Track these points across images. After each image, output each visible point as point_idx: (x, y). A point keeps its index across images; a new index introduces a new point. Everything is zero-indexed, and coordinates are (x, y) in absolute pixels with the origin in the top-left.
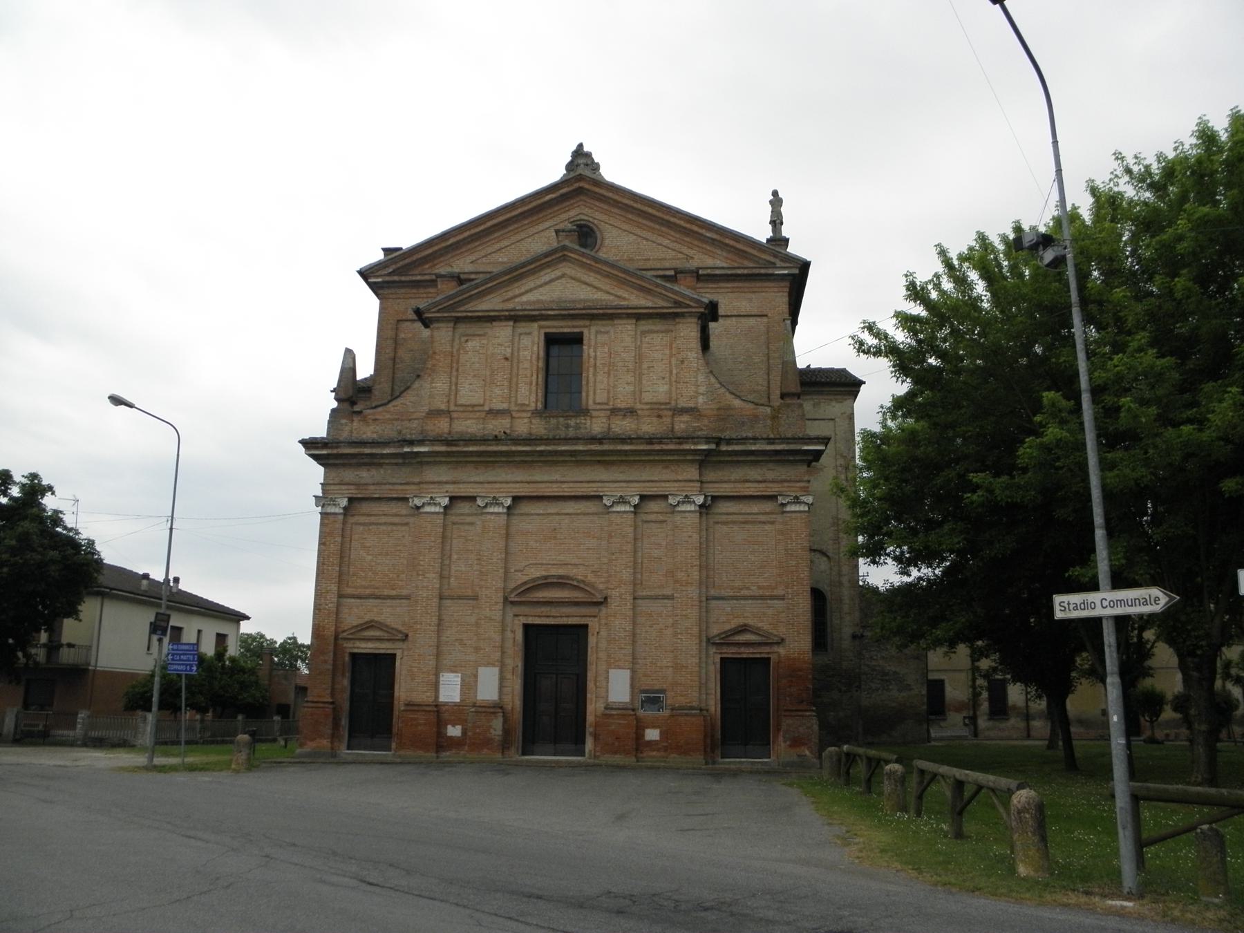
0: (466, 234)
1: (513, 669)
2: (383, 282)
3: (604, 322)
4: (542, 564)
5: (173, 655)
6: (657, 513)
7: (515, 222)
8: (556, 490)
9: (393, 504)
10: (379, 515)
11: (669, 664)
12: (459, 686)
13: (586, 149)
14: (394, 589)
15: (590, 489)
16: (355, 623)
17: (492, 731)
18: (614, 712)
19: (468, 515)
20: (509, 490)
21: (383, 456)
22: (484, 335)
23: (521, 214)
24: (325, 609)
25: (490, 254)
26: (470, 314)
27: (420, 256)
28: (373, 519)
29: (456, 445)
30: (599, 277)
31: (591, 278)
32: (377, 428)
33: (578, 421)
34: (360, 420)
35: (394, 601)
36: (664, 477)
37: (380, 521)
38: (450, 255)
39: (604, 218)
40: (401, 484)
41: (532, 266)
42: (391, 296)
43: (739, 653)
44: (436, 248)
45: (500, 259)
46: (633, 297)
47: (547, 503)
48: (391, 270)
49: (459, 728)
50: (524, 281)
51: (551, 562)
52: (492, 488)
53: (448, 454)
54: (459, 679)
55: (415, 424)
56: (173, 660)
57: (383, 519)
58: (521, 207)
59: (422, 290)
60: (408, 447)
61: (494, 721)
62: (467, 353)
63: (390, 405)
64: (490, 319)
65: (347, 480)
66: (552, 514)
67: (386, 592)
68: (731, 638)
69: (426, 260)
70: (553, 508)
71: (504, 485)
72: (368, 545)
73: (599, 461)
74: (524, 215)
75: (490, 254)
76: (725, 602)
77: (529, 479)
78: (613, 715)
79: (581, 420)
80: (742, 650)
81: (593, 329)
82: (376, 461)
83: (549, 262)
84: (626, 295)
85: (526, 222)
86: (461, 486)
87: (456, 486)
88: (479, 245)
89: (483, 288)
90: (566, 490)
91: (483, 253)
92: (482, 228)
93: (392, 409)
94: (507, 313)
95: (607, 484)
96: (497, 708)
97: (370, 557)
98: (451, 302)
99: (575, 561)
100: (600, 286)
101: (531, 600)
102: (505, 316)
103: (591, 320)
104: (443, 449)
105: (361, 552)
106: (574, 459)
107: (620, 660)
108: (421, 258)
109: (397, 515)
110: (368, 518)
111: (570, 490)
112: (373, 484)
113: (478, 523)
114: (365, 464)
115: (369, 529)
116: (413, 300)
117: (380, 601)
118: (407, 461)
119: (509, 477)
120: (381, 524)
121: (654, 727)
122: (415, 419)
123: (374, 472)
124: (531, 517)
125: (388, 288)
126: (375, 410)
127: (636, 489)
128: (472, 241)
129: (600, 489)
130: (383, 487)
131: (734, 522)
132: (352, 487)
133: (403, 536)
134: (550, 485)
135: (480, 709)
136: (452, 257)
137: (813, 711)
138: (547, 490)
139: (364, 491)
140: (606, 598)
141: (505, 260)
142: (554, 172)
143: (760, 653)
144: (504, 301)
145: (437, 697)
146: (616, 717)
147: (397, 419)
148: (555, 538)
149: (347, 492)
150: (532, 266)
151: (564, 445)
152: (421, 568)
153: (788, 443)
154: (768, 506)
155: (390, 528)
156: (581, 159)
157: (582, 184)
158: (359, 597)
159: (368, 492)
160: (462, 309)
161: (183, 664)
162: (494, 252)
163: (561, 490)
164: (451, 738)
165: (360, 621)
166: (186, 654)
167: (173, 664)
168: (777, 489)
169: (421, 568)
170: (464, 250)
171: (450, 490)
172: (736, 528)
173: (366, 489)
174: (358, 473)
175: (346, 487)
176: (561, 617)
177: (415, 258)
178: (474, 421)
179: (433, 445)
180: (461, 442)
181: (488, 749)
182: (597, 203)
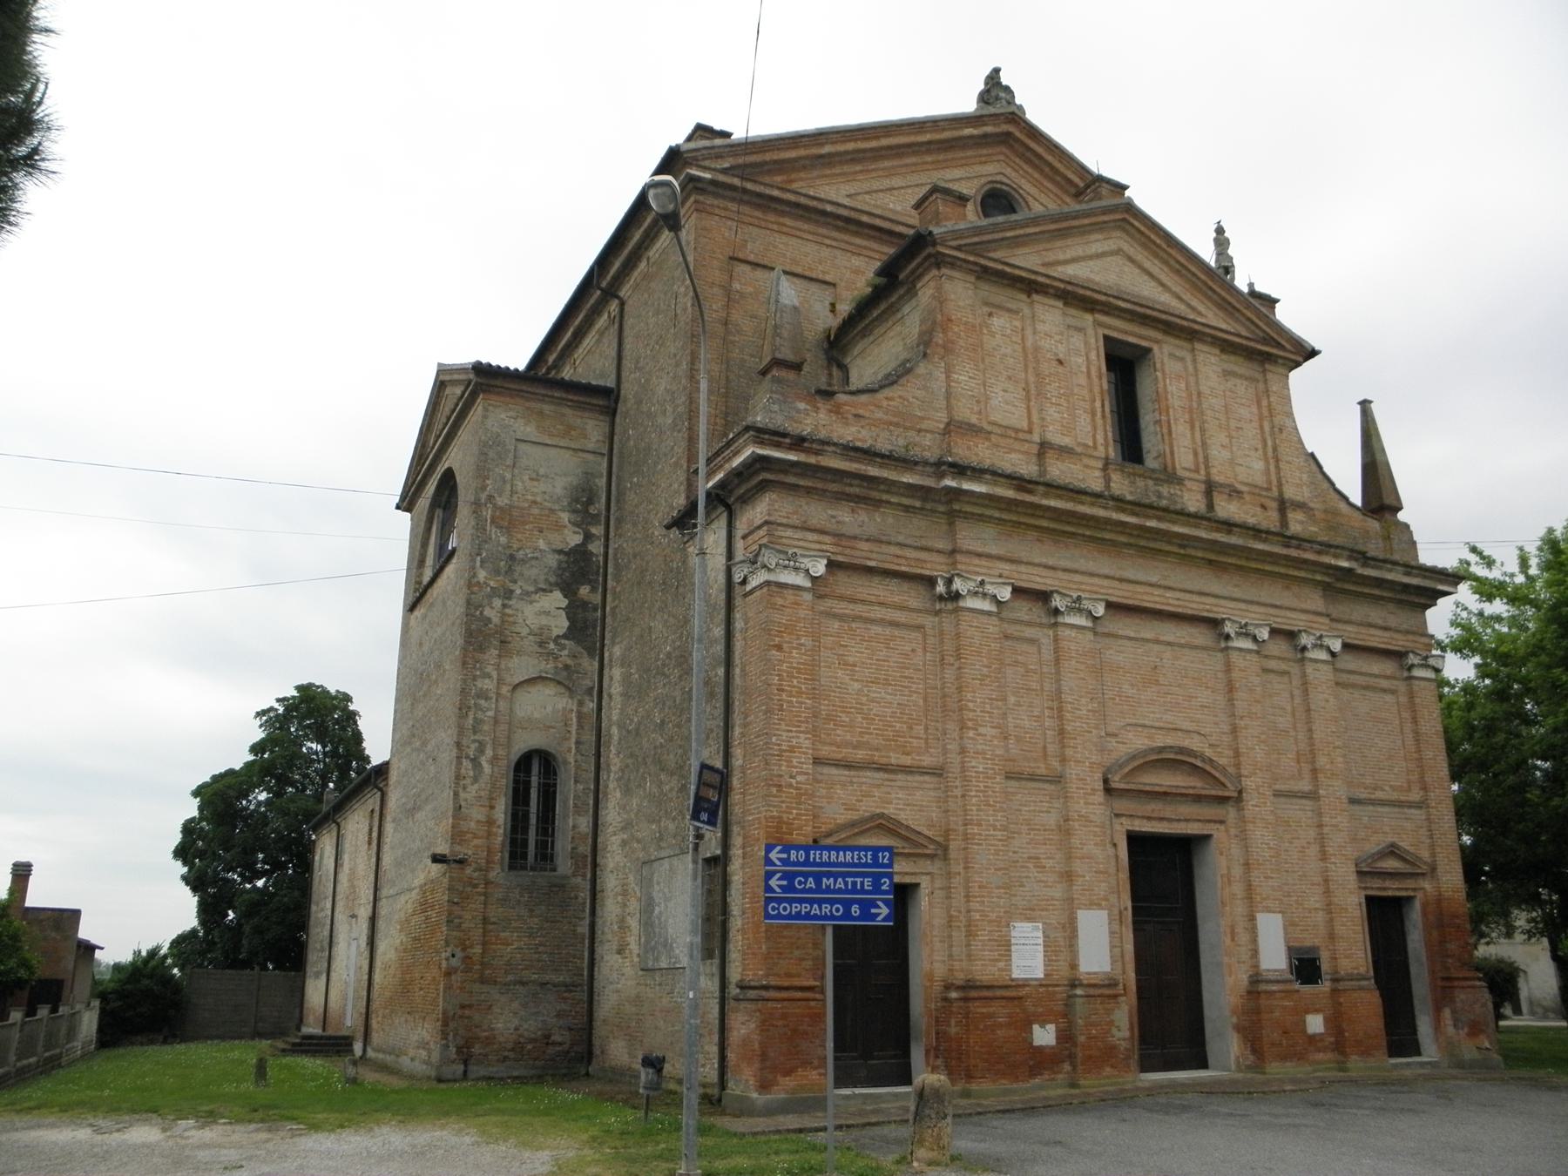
0: (850, 146)
1: (1120, 912)
2: (713, 182)
3: (1177, 342)
4: (1144, 726)
5: (786, 875)
6: (1279, 658)
7: (915, 153)
8: (1157, 599)
9: (894, 584)
10: (871, 603)
11: (1317, 906)
12: (1041, 948)
13: (1004, 81)
14: (908, 754)
15: (1202, 606)
16: (841, 819)
17: (1114, 1031)
18: (1274, 988)
19: (1029, 624)
20: (1095, 589)
21: (891, 485)
22: (1016, 312)
23: (929, 143)
24: (791, 786)
25: (876, 191)
26: (1008, 269)
27: (775, 157)
28: (859, 609)
29: (1030, 492)
30: (1166, 269)
31: (1155, 267)
32: (864, 432)
33: (1172, 491)
34: (831, 411)
35: (910, 778)
36: (1286, 602)
37: (872, 615)
38: (815, 173)
39: (1033, 190)
40: (916, 548)
41: (1086, 221)
42: (717, 211)
43: (1385, 889)
44: (802, 152)
45: (891, 206)
46: (1210, 315)
47: (1137, 621)
48: (726, 165)
49: (1051, 1028)
50: (1069, 241)
51: (1157, 724)
52: (1070, 581)
53: (1010, 504)
54: (1040, 934)
55: (927, 440)
56: (789, 888)
57: (879, 613)
58: (930, 132)
59: (771, 217)
60: (953, 479)
61: (1116, 1011)
62: (993, 335)
63: (880, 395)
64: (1030, 286)
65: (813, 522)
66: (1148, 640)
67: (895, 758)
68: (1379, 864)
69: (781, 166)
70: (1149, 629)
71: (1086, 579)
72: (851, 659)
73: (1210, 562)
74: (929, 147)
75: (876, 191)
76: (1361, 808)
77: (1118, 574)
78: (1275, 992)
79: (1175, 490)
80: (1388, 884)
81: (1166, 349)
82: (875, 494)
83: (1105, 222)
84: (1201, 308)
85: (929, 159)
86: (1023, 568)
87: (1014, 567)
88: (861, 172)
89: (1021, 232)
90: (1171, 601)
91: (866, 186)
92: (874, 144)
93: (885, 403)
94: (1062, 286)
95: (1222, 602)
96: (1105, 989)
97: (856, 685)
98: (976, 239)
99: (1186, 725)
100: (1169, 284)
101: (1141, 787)
102: (1057, 289)
103: (1166, 332)
104: (1010, 493)
105: (840, 673)
106: (1182, 551)
107: (1268, 898)
108: (775, 162)
109: (902, 608)
110: (851, 606)
111: (1176, 603)
112: (867, 540)
113: (1043, 641)
114: (849, 497)
115: (851, 629)
116: (756, 229)
117: (881, 775)
118: (928, 506)
119: (1091, 566)
120: (872, 621)
121: (1317, 1011)
122: (926, 431)
123: (863, 516)
124: (1120, 642)
125: (716, 195)
126: (854, 398)
127: (1257, 616)
128: (853, 161)
129: (1215, 609)
130: (885, 549)
131: (1354, 686)
132: (827, 539)
133: (913, 651)
134: (1149, 589)
135: (1092, 991)
136: (818, 177)
137: (1479, 979)
138: (1145, 598)
139: (848, 551)
140: (1240, 792)
141: (899, 208)
142: (965, 102)
143: (1407, 889)
144: (1043, 265)
145: (1074, 966)
146: (1278, 995)
147: (897, 425)
148: (1157, 682)
149: (818, 546)
150: (1086, 221)
151: (1184, 525)
152: (971, 715)
153: (1425, 577)
154: (1388, 667)
155: (888, 631)
156: (994, 88)
157: (1011, 128)
158: (849, 766)
159: (858, 553)
160: (997, 255)
161: (832, 902)
162: (882, 191)
163: (1165, 601)
164: (1040, 1049)
165: (853, 816)
166: (844, 875)
167: (791, 901)
168: (1401, 643)
169: (971, 715)
170: (837, 170)
171: (1006, 573)
172: (1357, 694)
173: (853, 548)
174: (834, 513)
175: (815, 537)
176: (1179, 820)
177: (768, 157)
178: (1021, 456)
179: (995, 484)
180: (1041, 488)
181: (1112, 1067)
182: (1026, 167)
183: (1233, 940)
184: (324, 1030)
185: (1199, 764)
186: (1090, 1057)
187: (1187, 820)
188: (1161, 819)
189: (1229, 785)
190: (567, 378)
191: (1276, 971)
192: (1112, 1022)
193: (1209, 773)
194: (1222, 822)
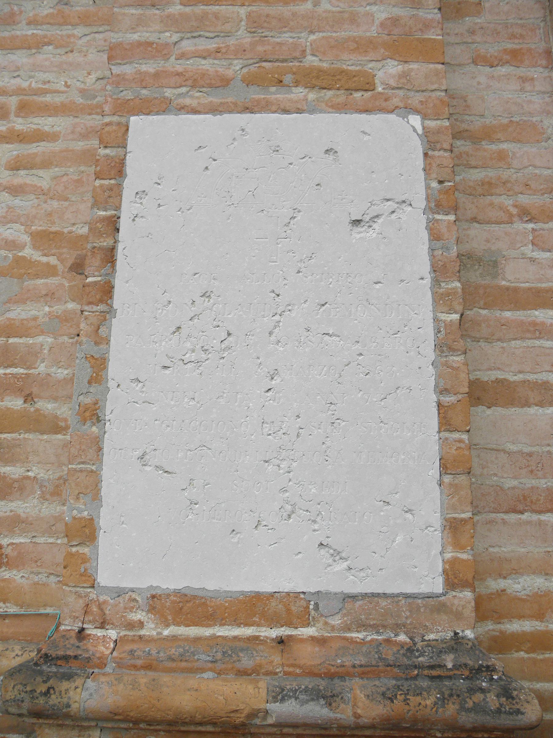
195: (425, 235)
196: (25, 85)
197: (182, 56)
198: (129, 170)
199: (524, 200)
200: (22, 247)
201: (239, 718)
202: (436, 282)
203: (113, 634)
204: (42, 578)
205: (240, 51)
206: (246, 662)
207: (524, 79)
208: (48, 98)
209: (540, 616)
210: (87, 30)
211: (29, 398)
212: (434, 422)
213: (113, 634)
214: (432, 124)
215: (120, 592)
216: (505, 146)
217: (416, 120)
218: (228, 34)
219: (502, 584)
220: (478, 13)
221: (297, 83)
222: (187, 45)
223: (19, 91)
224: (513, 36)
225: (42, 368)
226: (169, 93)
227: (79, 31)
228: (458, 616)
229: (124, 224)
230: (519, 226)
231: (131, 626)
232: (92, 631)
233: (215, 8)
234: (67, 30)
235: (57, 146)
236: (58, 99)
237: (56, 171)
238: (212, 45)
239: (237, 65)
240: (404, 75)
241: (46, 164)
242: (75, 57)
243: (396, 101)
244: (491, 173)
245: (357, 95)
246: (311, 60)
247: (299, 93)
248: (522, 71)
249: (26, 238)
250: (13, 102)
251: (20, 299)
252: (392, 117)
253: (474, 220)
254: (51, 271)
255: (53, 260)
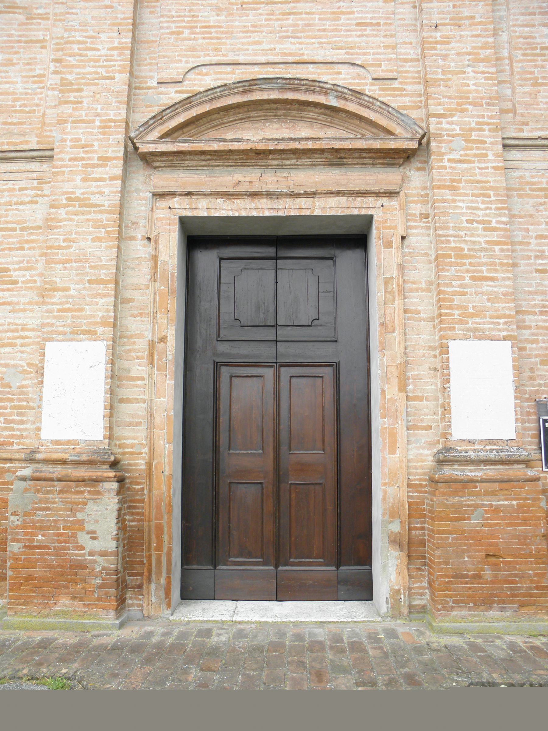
1: (152, 345)
17: (83, 538)
61: (90, 506)
78: (473, 481)
135: (48, 470)
183: (403, 387)
184: (138, 424)
185: (333, 102)
186: (29, 578)
187: (313, 194)
188: (255, 195)
189: (398, 130)
190: (431, 144)
191: (490, 442)
192: (81, 524)
193: (361, 118)
194: (391, 194)
195: (104, 370)
196: (22, 323)
197: (57, 326)
198: (46, 355)
199: (138, 354)
200: (24, 367)
201: (64, 460)
202: (106, 380)
203: (44, 448)
204: (32, 441)
205: (69, 325)
206: (66, 451)
207: (142, 321)
208: (28, 327)
209: (132, 448)
210: (37, 307)
211: (28, 402)
212: (103, 408)
213: (44, 448)
214: (108, 343)
215: (45, 440)
216: (135, 340)
217: (105, 342)
218: (67, 321)
219: (125, 441)
220: (133, 302)
221: (81, 334)
222: (58, 324)
223: (21, 324)
224: (141, 309)
225: (30, 396)
226: (54, 336)
227: (35, 307)
228: (105, 444)
229: (45, 367)
230: (136, 361)
231: (47, 446)
232: (40, 447)
233: (64, 314)
234: (32, 307)
235: (31, 340)
236: (31, 327)
237: (31, 347)
238: (63, 324)
239: (68, 329)
240: (104, 331)
241: (29, 345)
242: (34, 315)
243: (101, 338)
244: (131, 347)
245: (93, 336)
246: (84, 327)
247: (81, 336)
248: (142, 319)
249: (25, 365)
250: (20, 327)
251: (25, 380)
252: (100, 342)
253: (126, 360)
254: (31, 373)
255: (32, 370)
